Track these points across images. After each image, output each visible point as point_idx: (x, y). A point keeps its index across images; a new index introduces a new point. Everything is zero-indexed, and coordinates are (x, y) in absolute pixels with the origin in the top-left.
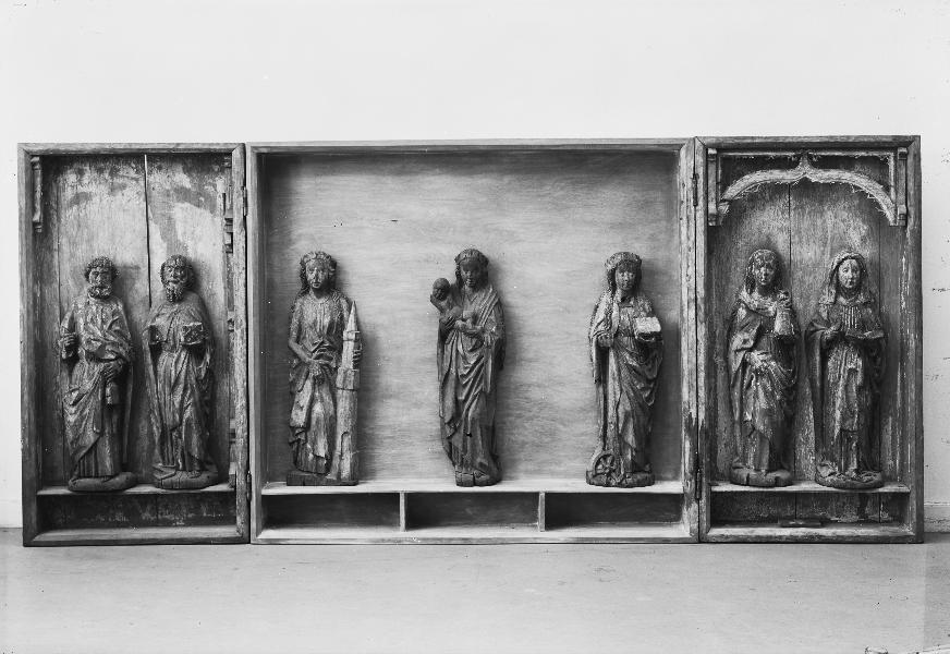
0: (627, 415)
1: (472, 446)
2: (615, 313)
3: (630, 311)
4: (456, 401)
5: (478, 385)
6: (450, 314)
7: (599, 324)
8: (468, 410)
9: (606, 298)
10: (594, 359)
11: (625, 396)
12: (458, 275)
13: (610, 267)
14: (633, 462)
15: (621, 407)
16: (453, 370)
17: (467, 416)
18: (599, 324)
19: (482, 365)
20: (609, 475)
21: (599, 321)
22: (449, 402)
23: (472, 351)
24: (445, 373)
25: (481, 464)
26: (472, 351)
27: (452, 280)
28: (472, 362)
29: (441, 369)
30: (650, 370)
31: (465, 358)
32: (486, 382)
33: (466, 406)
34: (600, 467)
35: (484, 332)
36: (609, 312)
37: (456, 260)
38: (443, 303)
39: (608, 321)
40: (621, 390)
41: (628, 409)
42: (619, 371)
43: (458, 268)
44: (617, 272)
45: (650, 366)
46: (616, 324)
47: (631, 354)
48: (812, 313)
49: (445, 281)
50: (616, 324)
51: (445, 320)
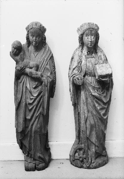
0: (92, 127)
1: (34, 147)
2: (83, 62)
3: (93, 60)
4: (25, 120)
5: (33, 107)
6: (21, 65)
7: (74, 69)
8: (32, 125)
9: (78, 52)
10: (71, 90)
11: (90, 114)
12: (28, 38)
13: (80, 33)
14: (96, 153)
15: (88, 122)
16: (23, 100)
17: (32, 128)
18: (74, 69)
19: (42, 97)
20: (82, 161)
21: (74, 67)
22: (21, 120)
23: (35, 88)
24: (18, 102)
25: (40, 157)
26: (35, 88)
27: (24, 42)
28: (36, 95)
29: (16, 99)
30: (105, 97)
31: (31, 92)
32: (43, 108)
33: (31, 124)
34: (77, 154)
35: (42, 76)
36: (80, 62)
37: (26, 29)
38: (18, 58)
39: (79, 67)
40: (88, 111)
41: (92, 122)
42: (87, 99)
43: (28, 34)
44: (84, 36)
45: (105, 95)
46: (84, 69)
47: (94, 88)
48: (32, 63)
49: (20, 43)
50: (84, 69)
51: (19, 68)
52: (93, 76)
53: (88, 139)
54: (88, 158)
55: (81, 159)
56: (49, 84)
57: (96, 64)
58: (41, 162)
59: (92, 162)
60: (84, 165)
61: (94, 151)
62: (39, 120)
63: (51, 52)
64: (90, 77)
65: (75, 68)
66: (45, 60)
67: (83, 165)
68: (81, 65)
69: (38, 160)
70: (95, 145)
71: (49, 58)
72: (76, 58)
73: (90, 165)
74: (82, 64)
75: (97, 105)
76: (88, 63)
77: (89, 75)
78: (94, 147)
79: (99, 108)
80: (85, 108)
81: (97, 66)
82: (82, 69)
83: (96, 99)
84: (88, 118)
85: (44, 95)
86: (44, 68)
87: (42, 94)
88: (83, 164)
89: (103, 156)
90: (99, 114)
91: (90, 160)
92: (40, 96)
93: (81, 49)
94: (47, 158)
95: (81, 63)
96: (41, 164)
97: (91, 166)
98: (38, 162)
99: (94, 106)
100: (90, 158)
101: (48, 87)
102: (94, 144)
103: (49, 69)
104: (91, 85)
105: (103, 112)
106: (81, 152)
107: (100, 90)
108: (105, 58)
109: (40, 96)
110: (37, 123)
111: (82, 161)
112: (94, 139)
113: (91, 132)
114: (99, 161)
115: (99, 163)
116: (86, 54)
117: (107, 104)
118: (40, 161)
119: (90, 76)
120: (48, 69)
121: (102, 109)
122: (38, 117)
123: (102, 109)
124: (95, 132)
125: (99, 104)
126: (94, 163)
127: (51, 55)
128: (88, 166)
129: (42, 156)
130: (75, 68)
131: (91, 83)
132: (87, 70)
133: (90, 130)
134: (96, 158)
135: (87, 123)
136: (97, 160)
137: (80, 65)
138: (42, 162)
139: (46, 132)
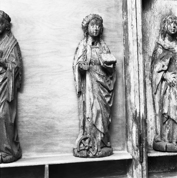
7: (79, 58)
9: (83, 42)
11: (96, 100)
18: (79, 58)
20: (88, 150)
21: (79, 56)
25: (7, 149)
32: (9, 94)
40: (94, 97)
46: (89, 58)
50: (89, 58)
52: (98, 65)
53: (94, 125)
54: (95, 146)
55: (87, 148)
56: (14, 70)
57: (101, 53)
58: (8, 154)
59: (99, 150)
60: (91, 155)
61: (100, 140)
62: (4, 106)
63: (16, 40)
64: (95, 66)
65: (80, 57)
66: (10, 47)
67: (89, 154)
68: (86, 54)
69: (5, 152)
70: (101, 132)
71: (14, 46)
72: (81, 49)
73: (96, 153)
74: (87, 53)
75: (102, 92)
76: (93, 53)
77: (93, 64)
78: (100, 134)
79: (104, 95)
80: (91, 95)
81: (102, 55)
82: (86, 58)
83: (101, 86)
84: (94, 104)
85: (9, 80)
86: (8, 55)
87: (6, 80)
88: (89, 153)
89: (108, 147)
90: (105, 101)
91: (96, 148)
92: (5, 83)
93: (85, 39)
94: (16, 151)
95: (86, 52)
96: (9, 157)
97: (97, 154)
98: (5, 154)
99: (100, 92)
100: (96, 146)
101: (13, 73)
102: (100, 131)
103: (14, 55)
104: (97, 73)
105: (108, 99)
106: (87, 141)
107: (105, 78)
108: (108, 50)
109: (5, 83)
110: (2, 110)
111: (88, 150)
112: (100, 127)
113: (97, 118)
114: (105, 150)
115: (105, 152)
116: (91, 44)
117: (112, 92)
118: (6, 153)
119: (95, 64)
120: (12, 56)
121: (107, 96)
122: (3, 104)
123: (107, 96)
124: (101, 119)
125: (104, 91)
126: (100, 151)
127: (16, 43)
128: (94, 154)
129: (10, 148)
130: (80, 57)
131: (96, 70)
132: (92, 58)
133: (97, 116)
134: (101, 148)
135: (93, 110)
136: (103, 149)
137: (85, 54)
138: (9, 154)
139: (13, 122)
